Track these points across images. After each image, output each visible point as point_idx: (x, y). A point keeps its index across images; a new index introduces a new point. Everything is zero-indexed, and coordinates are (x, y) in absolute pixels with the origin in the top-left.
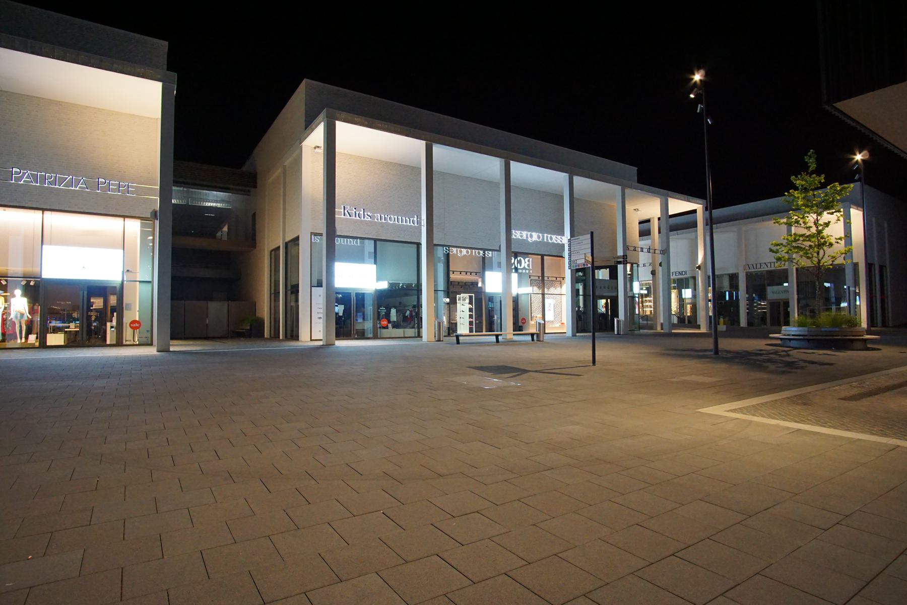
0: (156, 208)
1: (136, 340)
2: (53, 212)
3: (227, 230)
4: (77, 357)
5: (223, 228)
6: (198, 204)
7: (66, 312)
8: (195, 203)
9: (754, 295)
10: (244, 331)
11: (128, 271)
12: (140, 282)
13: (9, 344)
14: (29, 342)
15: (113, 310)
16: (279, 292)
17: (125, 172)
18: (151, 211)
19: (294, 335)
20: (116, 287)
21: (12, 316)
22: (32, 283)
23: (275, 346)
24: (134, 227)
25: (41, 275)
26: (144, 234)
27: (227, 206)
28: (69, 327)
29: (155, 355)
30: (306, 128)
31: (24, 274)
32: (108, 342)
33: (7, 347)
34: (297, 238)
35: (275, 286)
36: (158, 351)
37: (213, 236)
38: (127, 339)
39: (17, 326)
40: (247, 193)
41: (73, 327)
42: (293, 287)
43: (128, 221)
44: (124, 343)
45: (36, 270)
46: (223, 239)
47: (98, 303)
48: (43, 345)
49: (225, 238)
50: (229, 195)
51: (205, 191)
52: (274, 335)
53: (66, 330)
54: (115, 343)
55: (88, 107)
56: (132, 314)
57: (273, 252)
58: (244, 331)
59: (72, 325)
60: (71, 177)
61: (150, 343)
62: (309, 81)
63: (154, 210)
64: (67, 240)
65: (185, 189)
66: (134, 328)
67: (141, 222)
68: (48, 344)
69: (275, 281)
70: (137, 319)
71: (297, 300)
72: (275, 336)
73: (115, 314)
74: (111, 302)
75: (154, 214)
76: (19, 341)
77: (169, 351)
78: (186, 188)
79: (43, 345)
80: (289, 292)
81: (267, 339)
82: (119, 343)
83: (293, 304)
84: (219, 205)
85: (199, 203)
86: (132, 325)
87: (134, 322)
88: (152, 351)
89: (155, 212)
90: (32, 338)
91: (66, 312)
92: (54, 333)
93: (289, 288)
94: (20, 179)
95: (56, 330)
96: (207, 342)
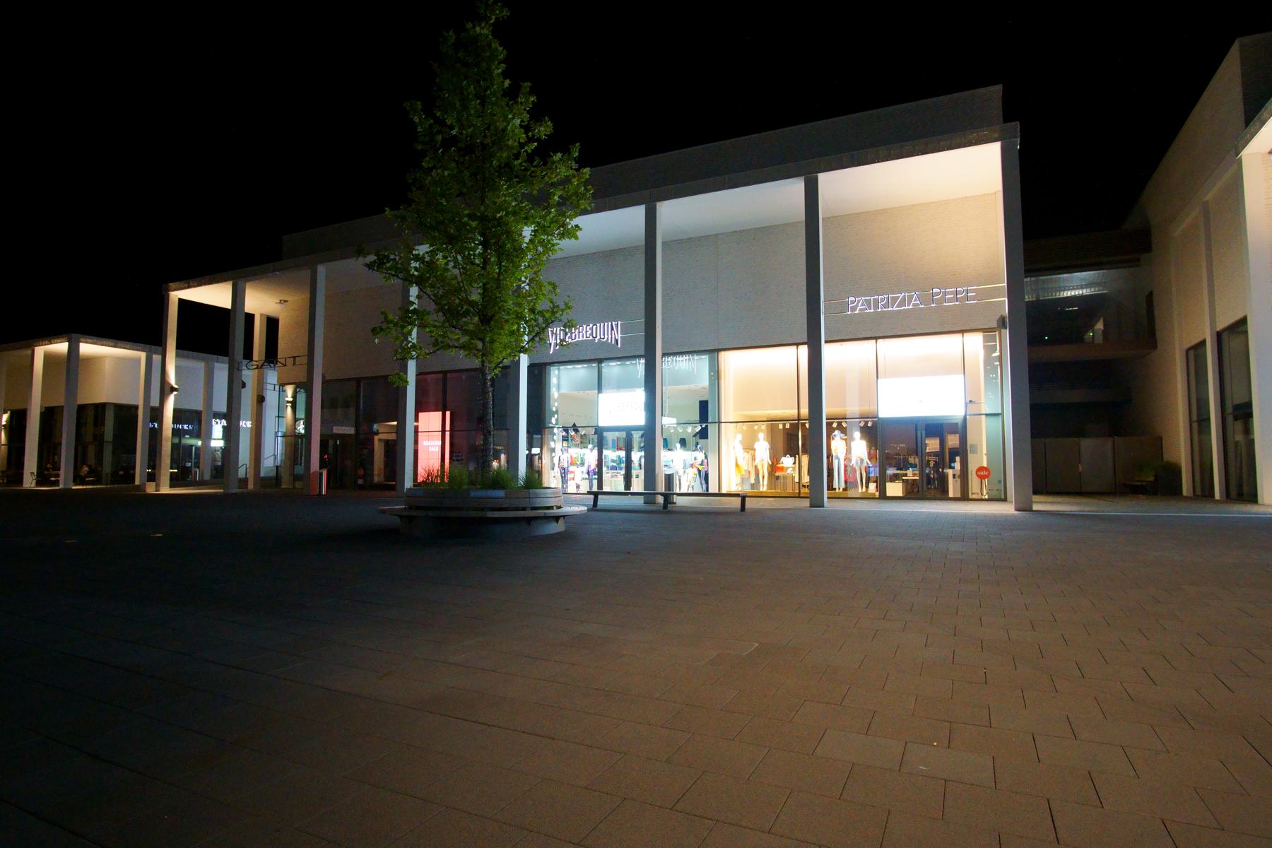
0: (1003, 314)
1: (985, 492)
2: (870, 341)
3: (1102, 328)
4: (921, 512)
5: (1094, 326)
6: (1056, 295)
7: (902, 457)
8: (1048, 296)
9: (536, 144)
10: (1145, 483)
11: (971, 401)
12: (987, 415)
13: (851, 493)
14: (869, 492)
15: (954, 453)
16: (1209, 419)
17: (960, 274)
18: (998, 317)
19: (1245, 493)
20: (957, 424)
21: (853, 462)
22: (870, 424)
23: (1207, 512)
24: (975, 342)
25: (878, 415)
26: (989, 350)
27: (1099, 291)
28: (906, 475)
29: (1014, 515)
30: (1246, 127)
31: (861, 414)
32: (951, 495)
33: (849, 496)
34: (1243, 321)
35: (1199, 408)
36: (1016, 510)
37: (1080, 339)
38: (974, 492)
39: (858, 473)
40: (1134, 263)
41: (911, 474)
42: (1237, 408)
43: (968, 336)
44: (971, 496)
45: (873, 408)
46: (1096, 342)
47: (933, 445)
48: (883, 496)
49: (1099, 340)
50: (1104, 273)
51: (1065, 275)
52: (1203, 490)
53: (904, 478)
54: (959, 496)
55: (913, 205)
56: (980, 458)
57: (1191, 352)
58: (1145, 483)
59: (910, 472)
60: (903, 294)
61: (1003, 497)
62: (1247, 39)
63: (1001, 316)
64: (902, 371)
65: (1033, 279)
66: (982, 478)
67: (984, 337)
68: (888, 495)
69: (1198, 400)
70: (985, 465)
71: (1248, 430)
72: (1204, 492)
73: (958, 459)
74: (949, 443)
75: (1002, 323)
76: (860, 490)
77: (1031, 510)
78: (1033, 276)
79: (883, 496)
80: (1230, 419)
81: (1187, 498)
82: (964, 497)
83: (1239, 437)
84: (1084, 291)
85: (1054, 294)
86: (979, 473)
87: (981, 469)
88: (1008, 509)
89: (1002, 319)
90: (872, 486)
91: (902, 457)
92: (891, 482)
93: (1229, 409)
94: (854, 309)
95: (894, 478)
96: (1084, 500)
